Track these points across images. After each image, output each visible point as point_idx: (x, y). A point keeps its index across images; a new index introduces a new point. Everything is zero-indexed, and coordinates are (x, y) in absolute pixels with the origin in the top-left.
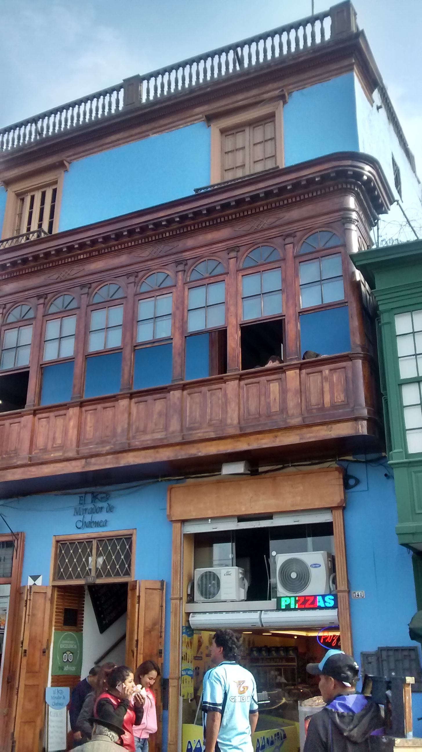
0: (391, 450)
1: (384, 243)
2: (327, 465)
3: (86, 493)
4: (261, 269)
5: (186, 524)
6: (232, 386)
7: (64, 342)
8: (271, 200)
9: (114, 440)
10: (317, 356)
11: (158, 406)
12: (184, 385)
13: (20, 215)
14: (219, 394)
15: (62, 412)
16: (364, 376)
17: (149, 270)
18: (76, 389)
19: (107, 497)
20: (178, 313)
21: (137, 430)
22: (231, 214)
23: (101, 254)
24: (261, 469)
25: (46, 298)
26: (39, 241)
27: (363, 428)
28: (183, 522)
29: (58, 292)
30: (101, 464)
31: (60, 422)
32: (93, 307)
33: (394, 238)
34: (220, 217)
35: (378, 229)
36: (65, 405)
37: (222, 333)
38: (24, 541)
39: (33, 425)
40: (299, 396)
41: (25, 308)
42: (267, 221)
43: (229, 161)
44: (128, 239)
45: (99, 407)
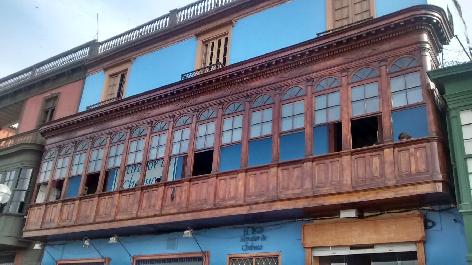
0: (460, 202)
1: (447, 64)
2: (411, 212)
3: (248, 227)
4: (327, 91)
5: (314, 250)
6: (346, 159)
7: (235, 132)
8: (369, 38)
9: (268, 194)
10: (409, 137)
11: (297, 172)
12: (314, 159)
13: (206, 55)
14: (338, 164)
15: (234, 176)
16: (439, 153)
17: (289, 85)
18: (243, 161)
19: (262, 230)
20: (308, 112)
21: (283, 188)
22: (343, 48)
23: (258, 77)
24: (365, 215)
25: (223, 105)
26: (218, 71)
27: (439, 188)
28: (313, 248)
29: (205, 108)
30: (260, 209)
31: (233, 182)
32: (253, 110)
33: (454, 61)
34: (336, 50)
35: (442, 55)
36: (236, 171)
37: (338, 126)
38: (209, 257)
39: (216, 183)
40: (393, 166)
41: (211, 111)
42: (367, 52)
43: (338, 15)
44: (275, 67)
45: (258, 172)
